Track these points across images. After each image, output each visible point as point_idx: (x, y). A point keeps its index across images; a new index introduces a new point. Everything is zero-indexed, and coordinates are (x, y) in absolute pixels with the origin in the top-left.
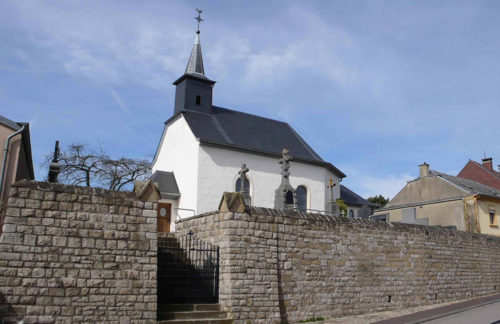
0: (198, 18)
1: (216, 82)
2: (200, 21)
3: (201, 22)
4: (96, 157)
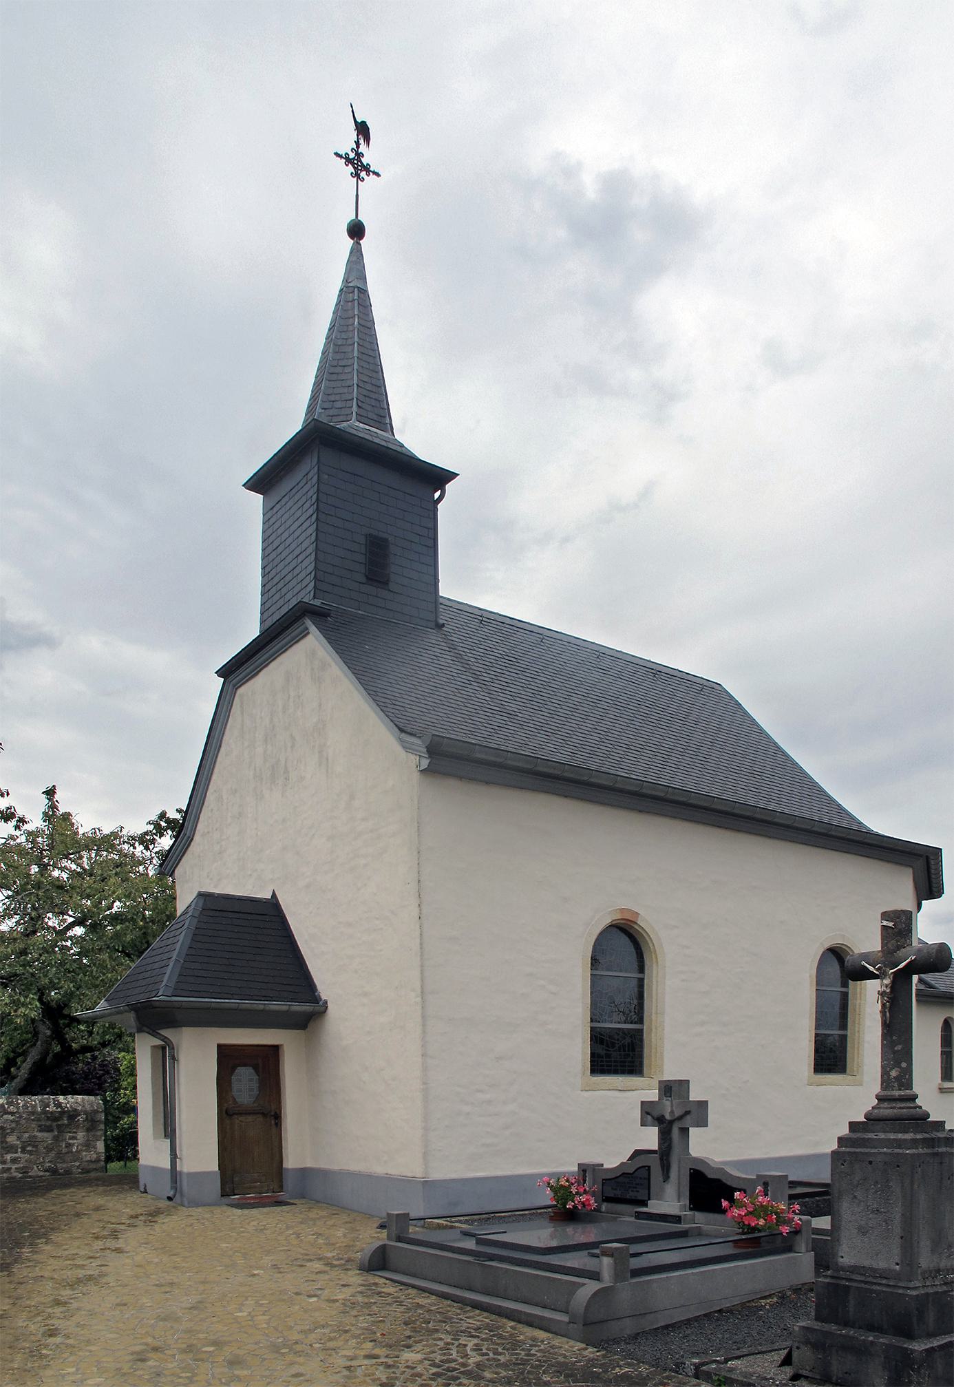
0: (352, 155)
1: (458, 475)
2: (363, 174)
3: (370, 180)
4: (142, 1214)
